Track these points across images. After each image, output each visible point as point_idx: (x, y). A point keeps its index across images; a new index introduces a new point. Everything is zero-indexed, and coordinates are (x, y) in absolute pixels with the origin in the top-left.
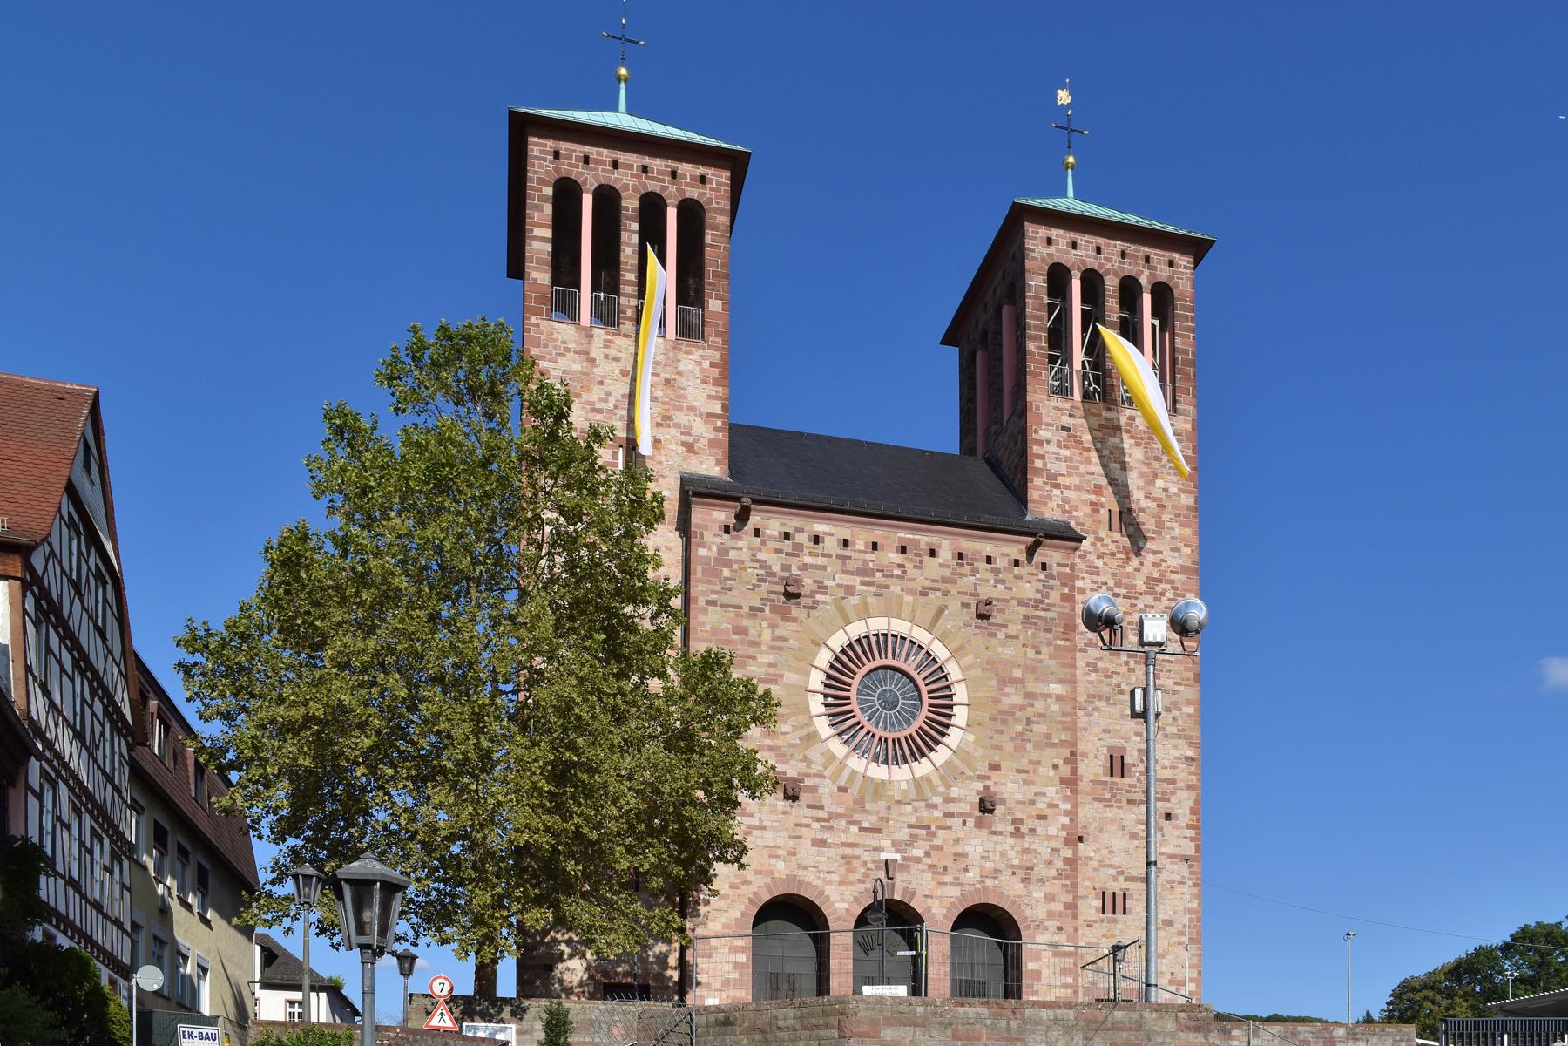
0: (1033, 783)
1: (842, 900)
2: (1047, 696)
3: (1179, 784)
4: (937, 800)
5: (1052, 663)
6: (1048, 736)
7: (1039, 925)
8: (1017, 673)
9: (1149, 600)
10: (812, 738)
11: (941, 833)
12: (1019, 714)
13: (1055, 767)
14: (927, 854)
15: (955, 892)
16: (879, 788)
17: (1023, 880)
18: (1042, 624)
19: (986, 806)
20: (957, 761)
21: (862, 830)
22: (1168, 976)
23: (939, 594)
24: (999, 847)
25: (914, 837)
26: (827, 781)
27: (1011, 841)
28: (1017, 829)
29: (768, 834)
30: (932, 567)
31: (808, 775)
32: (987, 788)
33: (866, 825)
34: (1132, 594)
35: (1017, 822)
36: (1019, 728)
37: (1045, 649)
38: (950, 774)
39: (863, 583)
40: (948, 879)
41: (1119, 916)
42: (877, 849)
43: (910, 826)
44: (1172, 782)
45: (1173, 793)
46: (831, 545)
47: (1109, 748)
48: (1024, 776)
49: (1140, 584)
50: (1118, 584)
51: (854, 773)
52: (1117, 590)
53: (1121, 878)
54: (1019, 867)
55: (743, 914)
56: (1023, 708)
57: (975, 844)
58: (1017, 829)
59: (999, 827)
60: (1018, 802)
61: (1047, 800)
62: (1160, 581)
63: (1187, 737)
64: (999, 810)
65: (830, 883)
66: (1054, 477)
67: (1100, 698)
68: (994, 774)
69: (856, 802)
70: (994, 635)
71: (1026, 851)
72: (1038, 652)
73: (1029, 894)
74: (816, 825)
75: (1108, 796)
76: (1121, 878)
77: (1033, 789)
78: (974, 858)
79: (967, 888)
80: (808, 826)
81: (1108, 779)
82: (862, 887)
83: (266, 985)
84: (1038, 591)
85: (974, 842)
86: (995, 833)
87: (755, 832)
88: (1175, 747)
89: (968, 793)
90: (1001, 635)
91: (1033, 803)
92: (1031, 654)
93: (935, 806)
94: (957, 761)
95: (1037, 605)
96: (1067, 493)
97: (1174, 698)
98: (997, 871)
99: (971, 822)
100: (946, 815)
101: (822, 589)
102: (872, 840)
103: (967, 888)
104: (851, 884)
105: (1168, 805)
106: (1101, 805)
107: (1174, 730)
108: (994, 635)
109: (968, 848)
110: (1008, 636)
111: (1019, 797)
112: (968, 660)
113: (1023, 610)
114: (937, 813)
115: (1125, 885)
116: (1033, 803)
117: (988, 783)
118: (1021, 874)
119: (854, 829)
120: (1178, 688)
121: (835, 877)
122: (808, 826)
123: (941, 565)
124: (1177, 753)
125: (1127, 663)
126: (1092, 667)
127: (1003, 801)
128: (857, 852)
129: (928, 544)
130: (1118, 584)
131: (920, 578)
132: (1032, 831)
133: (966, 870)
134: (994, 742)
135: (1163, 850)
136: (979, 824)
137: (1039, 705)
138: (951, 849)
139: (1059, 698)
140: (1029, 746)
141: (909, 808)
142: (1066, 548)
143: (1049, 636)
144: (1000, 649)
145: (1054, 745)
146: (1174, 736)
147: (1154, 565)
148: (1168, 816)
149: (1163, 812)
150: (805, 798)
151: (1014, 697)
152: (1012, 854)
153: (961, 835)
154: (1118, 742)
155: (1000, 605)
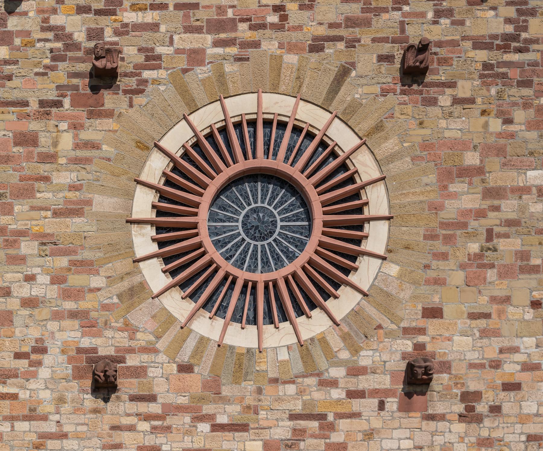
8: (472, 159)
10: (137, 292)
11: (343, 424)
12: (473, 224)
16: (242, 363)
18: (514, 74)
21: (217, 428)
23: (341, 46)
26: (162, 358)
27: (459, 427)
28: (470, 409)
33: (222, 419)
35: (469, 398)
36: (474, 247)
39: (217, 44)
43: (293, 417)
48: (482, 323)
51: (203, 341)
56: (481, 214)
58: (470, 409)
59: (439, 408)
60: (472, 366)
61: (519, 357)
69: (206, 386)
70: (432, 102)
72: (508, 121)
74: (144, 426)
77: (496, 343)
80: (131, 428)
84: (508, 21)
86: (432, 418)
90: (445, 100)
91: (496, 365)
93: (334, 383)
94: (371, 310)
99: (392, 404)
100: (352, 394)
101: (152, 60)
108: (432, 102)
110: (457, 101)
111: (473, 356)
112: (390, 145)
113: (482, 55)
114: (337, 394)
116: (496, 365)
117: (421, 339)
119: (204, 427)
122: (131, 428)
132: (496, 410)
136: (405, 408)
137: (509, 207)
140: (491, 274)
141: (291, 389)
143: (527, 92)
150: (127, 386)
151: (465, 198)
153: (376, 424)
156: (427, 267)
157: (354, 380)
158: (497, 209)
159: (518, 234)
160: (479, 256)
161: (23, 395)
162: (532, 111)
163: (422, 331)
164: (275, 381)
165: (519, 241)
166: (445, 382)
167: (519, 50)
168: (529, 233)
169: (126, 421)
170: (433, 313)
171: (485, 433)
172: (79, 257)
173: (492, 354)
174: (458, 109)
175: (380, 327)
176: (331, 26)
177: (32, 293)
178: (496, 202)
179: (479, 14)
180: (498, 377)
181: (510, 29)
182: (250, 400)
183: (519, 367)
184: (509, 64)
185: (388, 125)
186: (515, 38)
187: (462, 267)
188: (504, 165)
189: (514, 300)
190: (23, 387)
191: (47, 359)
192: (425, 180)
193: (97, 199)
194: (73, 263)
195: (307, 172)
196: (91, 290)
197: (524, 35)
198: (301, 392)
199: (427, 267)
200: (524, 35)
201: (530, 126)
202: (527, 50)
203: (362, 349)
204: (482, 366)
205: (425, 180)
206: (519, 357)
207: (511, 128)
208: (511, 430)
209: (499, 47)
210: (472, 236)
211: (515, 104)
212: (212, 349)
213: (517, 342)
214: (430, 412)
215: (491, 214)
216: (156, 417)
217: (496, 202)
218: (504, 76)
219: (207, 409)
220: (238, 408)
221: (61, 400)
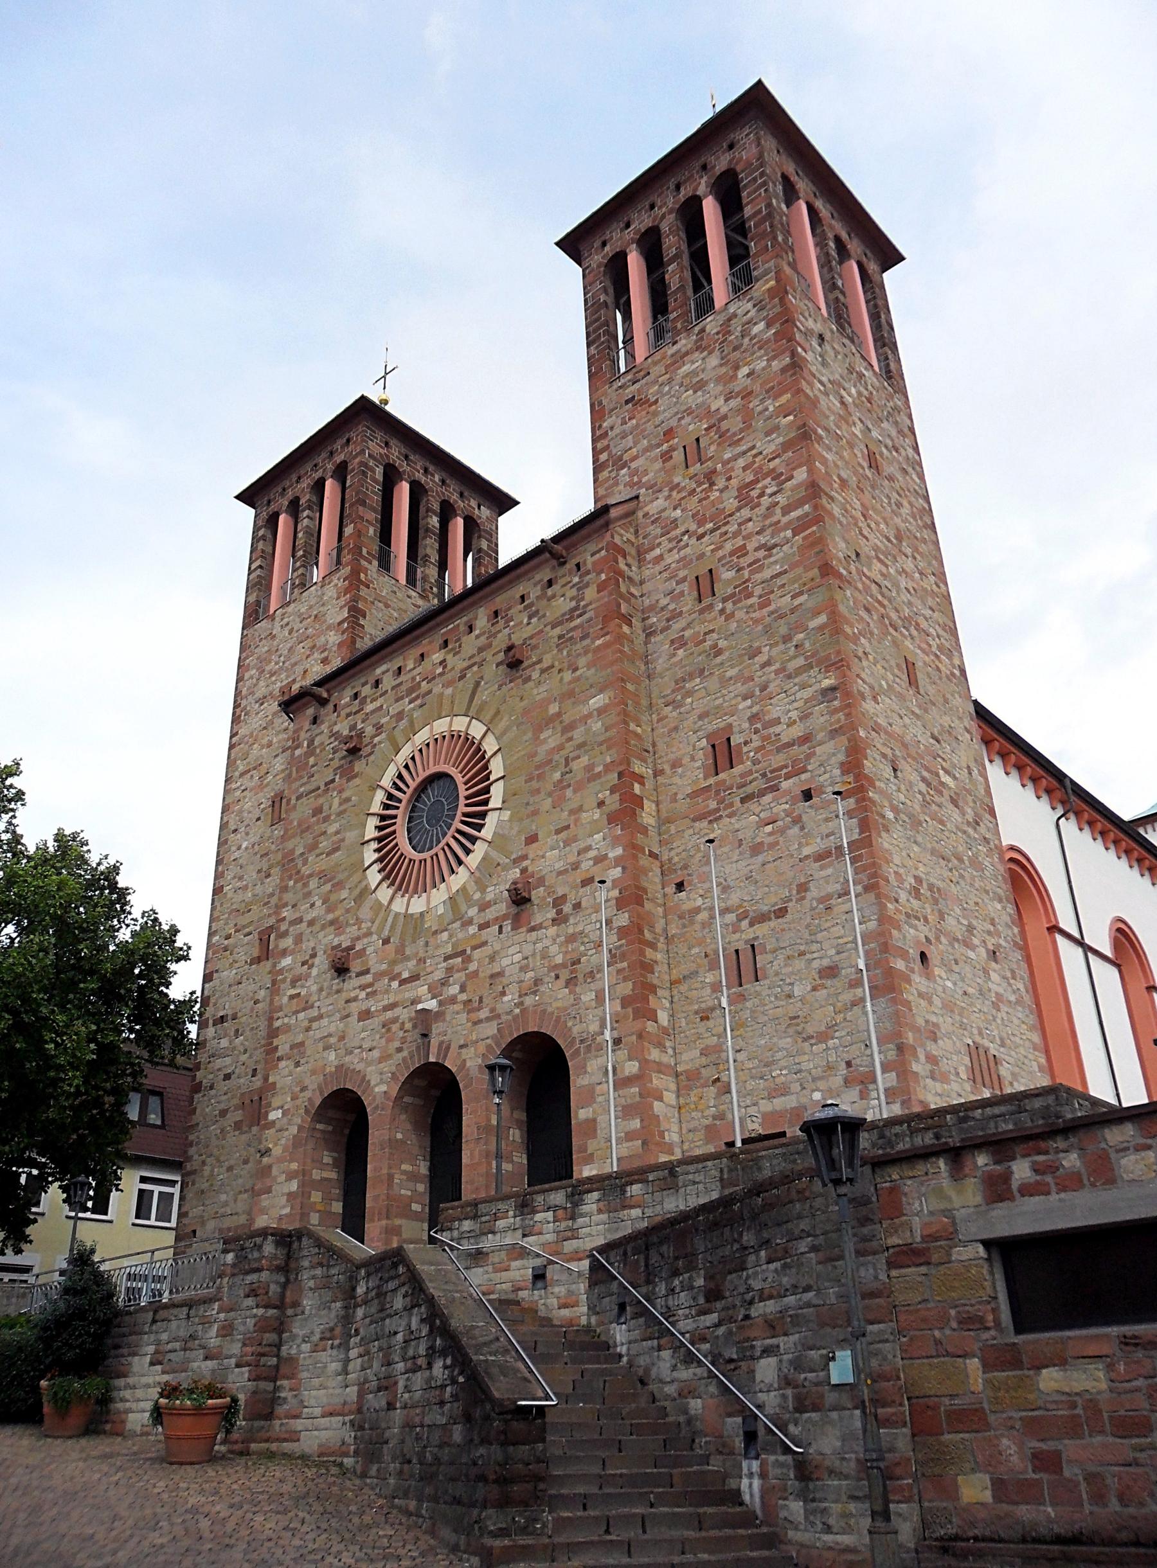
0: (575, 839)
1: (382, 1082)
2: (585, 719)
3: (820, 736)
4: (473, 912)
5: (593, 670)
6: (589, 768)
7: (592, 1045)
8: (553, 709)
9: (746, 513)
10: (365, 892)
11: (477, 954)
12: (556, 757)
13: (601, 804)
14: (463, 989)
15: (491, 1029)
16: (414, 923)
17: (568, 983)
18: (577, 634)
19: (520, 899)
20: (494, 854)
22: (843, 1070)
23: (475, 668)
24: (539, 946)
25: (449, 970)
26: (375, 937)
27: (552, 931)
28: (559, 912)
29: (325, 1022)
30: (470, 644)
31: (358, 938)
32: (524, 871)
33: (405, 975)
34: (721, 518)
35: (559, 902)
36: (557, 776)
37: (582, 662)
38: (482, 876)
40: (484, 1014)
41: (749, 987)
42: (414, 1002)
44: (806, 739)
45: (809, 756)
46: (388, 682)
47: (708, 737)
48: (564, 835)
49: (731, 503)
50: (701, 523)
51: (397, 914)
52: (701, 531)
53: (745, 923)
54: (563, 965)
55: (300, 1128)
56: (561, 747)
57: (512, 953)
58: (559, 912)
59: (538, 919)
60: (560, 873)
61: (592, 854)
62: (757, 481)
63: (819, 663)
64: (537, 894)
65: (369, 1063)
66: (620, 458)
67: (691, 676)
68: (532, 851)
69: (397, 952)
70: (529, 679)
71: (571, 938)
72: (576, 669)
73: (577, 999)
74: (363, 995)
75: (713, 805)
76: (745, 923)
77: (575, 847)
78: (512, 973)
79: (504, 1018)
80: (355, 999)
81: (712, 781)
82: (400, 1055)
83: (571, 1177)
84: (572, 599)
85: (511, 951)
86: (533, 929)
87: (315, 1025)
88: (803, 687)
89: (498, 890)
90: (535, 675)
91: (576, 866)
92: (568, 676)
93: (470, 922)
94: (494, 854)
95: (572, 614)
96: (633, 465)
97: (793, 618)
98: (537, 982)
99: (507, 928)
101: (379, 728)
102: (409, 993)
103: (504, 1018)
104: (390, 1056)
105: (803, 777)
106: (705, 823)
107: (801, 661)
108: (529, 679)
109: (505, 962)
110: (543, 671)
111: (559, 865)
112: (503, 724)
113: (558, 631)
114: (473, 929)
115: (750, 934)
116: (576, 866)
117: (525, 863)
118: (565, 975)
120: (796, 602)
121: (376, 1054)
123: (477, 637)
124: (807, 693)
125: (722, 611)
126: (679, 642)
127: (541, 881)
128: (398, 1011)
129: (466, 623)
130: (701, 523)
131: (456, 663)
132: (577, 906)
133: (503, 994)
134: (531, 808)
135: (806, 851)
136: (517, 922)
137: (578, 734)
138: (485, 973)
139: (601, 711)
140: (569, 793)
141: (445, 935)
142: (597, 531)
143: (587, 642)
144: (535, 692)
145: (599, 775)
146: (799, 671)
147: (745, 469)
148: (807, 795)
149: (797, 791)
150: (355, 966)
151: (551, 738)
152: (554, 949)
153: (497, 947)
154: (718, 724)
155: (533, 642)
156: (528, 804)
157: (483, 914)
158: (571, 739)
159: (586, 752)
160: (560, 781)
161: (304, 992)
162: (590, 655)
163: (525, 857)
164: (435, 933)
165: (587, 757)
166: (541, 895)
167: (580, 615)
168: (593, 749)
169: (353, 995)
170: (532, 839)
171: (571, 931)
172: (336, 881)
173: (572, 858)
174: (545, 675)
175: (499, 864)
176: (470, 658)
177: (690, 1204)
178: (570, 735)
179: (554, 604)
180: (578, 876)
181: (573, 604)
182: (421, 954)
183: (591, 863)
184: (573, 629)
185: (502, 709)
186: (576, 608)
187: (550, 794)
188: (574, 703)
189: (585, 807)
190: (303, 987)
191: (317, 961)
192: (525, 738)
193: (348, 834)
194: (333, 886)
195: (457, 835)
196: (341, 902)
197: (582, 603)
198: (451, 936)
199: (528, 804)
200: (582, 603)
201: (589, 666)
202: (585, 613)
203: (487, 887)
204: (566, 871)
205: (525, 738)
206: (592, 854)
207: (578, 673)
208: (589, 921)
209: (567, 620)
210: (554, 769)
211: (579, 655)
212: (402, 917)
213: (589, 841)
214: (533, 924)
215: (567, 745)
216: (371, 985)
217: (570, 735)
218: (572, 638)
219: (397, 969)
220: (414, 962)
221: (321, 990)
